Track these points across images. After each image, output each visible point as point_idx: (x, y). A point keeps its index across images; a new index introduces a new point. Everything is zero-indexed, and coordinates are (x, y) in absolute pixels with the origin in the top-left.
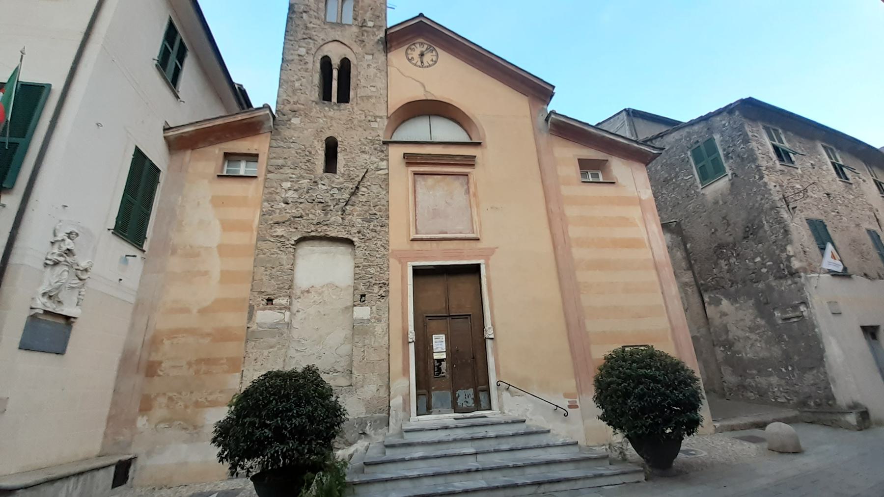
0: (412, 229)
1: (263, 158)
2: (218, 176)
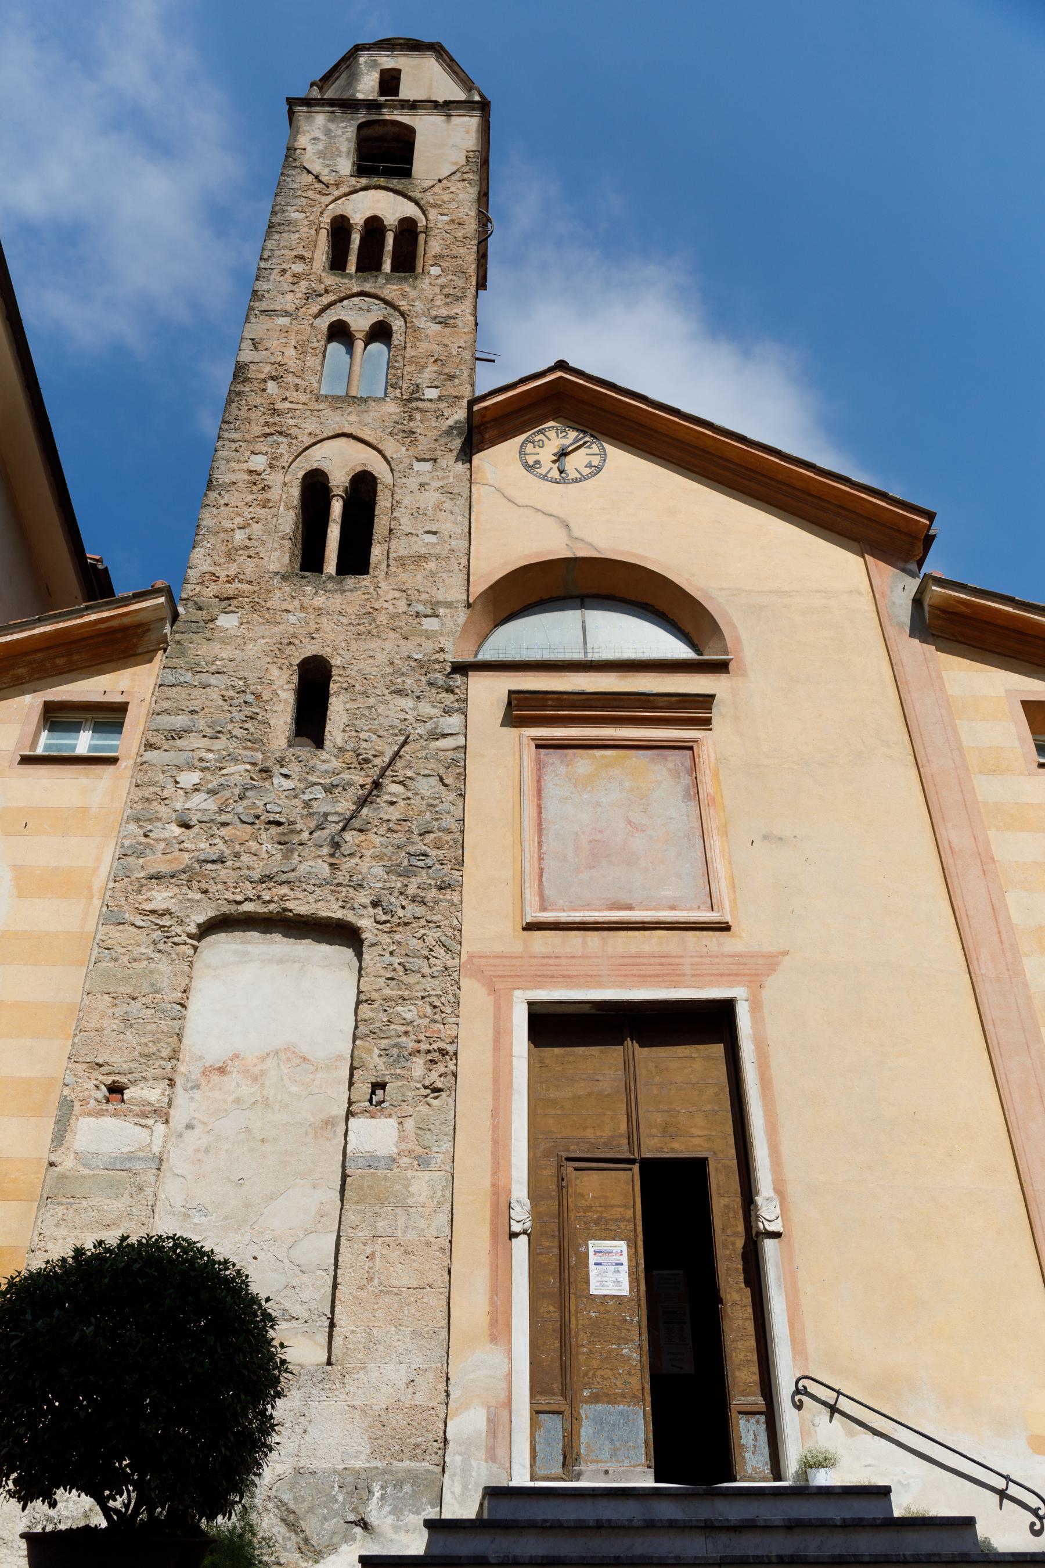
0: (531, 897)
1: (135, 722)
2: (26, 760)
